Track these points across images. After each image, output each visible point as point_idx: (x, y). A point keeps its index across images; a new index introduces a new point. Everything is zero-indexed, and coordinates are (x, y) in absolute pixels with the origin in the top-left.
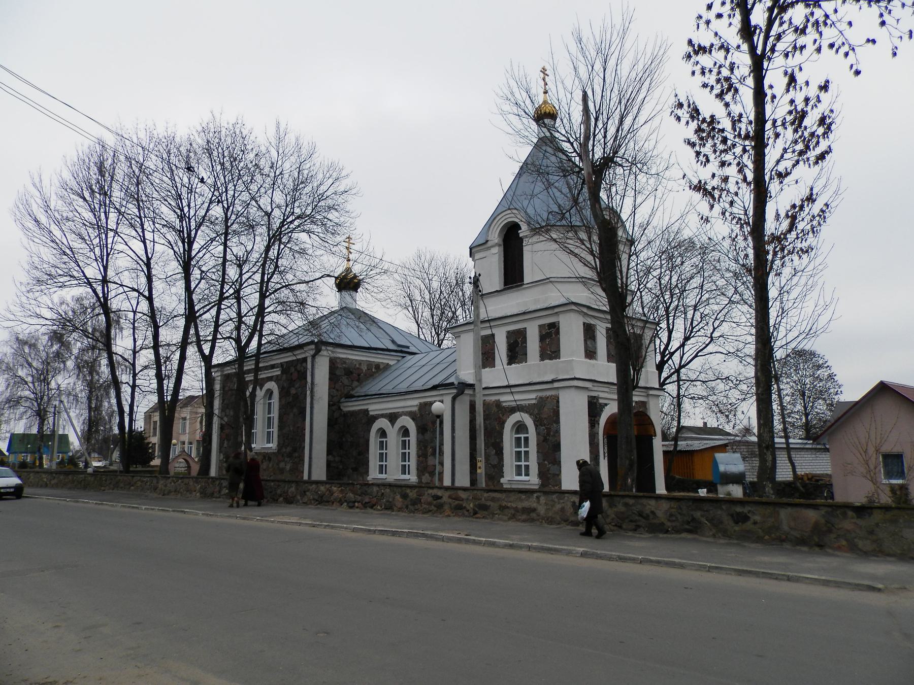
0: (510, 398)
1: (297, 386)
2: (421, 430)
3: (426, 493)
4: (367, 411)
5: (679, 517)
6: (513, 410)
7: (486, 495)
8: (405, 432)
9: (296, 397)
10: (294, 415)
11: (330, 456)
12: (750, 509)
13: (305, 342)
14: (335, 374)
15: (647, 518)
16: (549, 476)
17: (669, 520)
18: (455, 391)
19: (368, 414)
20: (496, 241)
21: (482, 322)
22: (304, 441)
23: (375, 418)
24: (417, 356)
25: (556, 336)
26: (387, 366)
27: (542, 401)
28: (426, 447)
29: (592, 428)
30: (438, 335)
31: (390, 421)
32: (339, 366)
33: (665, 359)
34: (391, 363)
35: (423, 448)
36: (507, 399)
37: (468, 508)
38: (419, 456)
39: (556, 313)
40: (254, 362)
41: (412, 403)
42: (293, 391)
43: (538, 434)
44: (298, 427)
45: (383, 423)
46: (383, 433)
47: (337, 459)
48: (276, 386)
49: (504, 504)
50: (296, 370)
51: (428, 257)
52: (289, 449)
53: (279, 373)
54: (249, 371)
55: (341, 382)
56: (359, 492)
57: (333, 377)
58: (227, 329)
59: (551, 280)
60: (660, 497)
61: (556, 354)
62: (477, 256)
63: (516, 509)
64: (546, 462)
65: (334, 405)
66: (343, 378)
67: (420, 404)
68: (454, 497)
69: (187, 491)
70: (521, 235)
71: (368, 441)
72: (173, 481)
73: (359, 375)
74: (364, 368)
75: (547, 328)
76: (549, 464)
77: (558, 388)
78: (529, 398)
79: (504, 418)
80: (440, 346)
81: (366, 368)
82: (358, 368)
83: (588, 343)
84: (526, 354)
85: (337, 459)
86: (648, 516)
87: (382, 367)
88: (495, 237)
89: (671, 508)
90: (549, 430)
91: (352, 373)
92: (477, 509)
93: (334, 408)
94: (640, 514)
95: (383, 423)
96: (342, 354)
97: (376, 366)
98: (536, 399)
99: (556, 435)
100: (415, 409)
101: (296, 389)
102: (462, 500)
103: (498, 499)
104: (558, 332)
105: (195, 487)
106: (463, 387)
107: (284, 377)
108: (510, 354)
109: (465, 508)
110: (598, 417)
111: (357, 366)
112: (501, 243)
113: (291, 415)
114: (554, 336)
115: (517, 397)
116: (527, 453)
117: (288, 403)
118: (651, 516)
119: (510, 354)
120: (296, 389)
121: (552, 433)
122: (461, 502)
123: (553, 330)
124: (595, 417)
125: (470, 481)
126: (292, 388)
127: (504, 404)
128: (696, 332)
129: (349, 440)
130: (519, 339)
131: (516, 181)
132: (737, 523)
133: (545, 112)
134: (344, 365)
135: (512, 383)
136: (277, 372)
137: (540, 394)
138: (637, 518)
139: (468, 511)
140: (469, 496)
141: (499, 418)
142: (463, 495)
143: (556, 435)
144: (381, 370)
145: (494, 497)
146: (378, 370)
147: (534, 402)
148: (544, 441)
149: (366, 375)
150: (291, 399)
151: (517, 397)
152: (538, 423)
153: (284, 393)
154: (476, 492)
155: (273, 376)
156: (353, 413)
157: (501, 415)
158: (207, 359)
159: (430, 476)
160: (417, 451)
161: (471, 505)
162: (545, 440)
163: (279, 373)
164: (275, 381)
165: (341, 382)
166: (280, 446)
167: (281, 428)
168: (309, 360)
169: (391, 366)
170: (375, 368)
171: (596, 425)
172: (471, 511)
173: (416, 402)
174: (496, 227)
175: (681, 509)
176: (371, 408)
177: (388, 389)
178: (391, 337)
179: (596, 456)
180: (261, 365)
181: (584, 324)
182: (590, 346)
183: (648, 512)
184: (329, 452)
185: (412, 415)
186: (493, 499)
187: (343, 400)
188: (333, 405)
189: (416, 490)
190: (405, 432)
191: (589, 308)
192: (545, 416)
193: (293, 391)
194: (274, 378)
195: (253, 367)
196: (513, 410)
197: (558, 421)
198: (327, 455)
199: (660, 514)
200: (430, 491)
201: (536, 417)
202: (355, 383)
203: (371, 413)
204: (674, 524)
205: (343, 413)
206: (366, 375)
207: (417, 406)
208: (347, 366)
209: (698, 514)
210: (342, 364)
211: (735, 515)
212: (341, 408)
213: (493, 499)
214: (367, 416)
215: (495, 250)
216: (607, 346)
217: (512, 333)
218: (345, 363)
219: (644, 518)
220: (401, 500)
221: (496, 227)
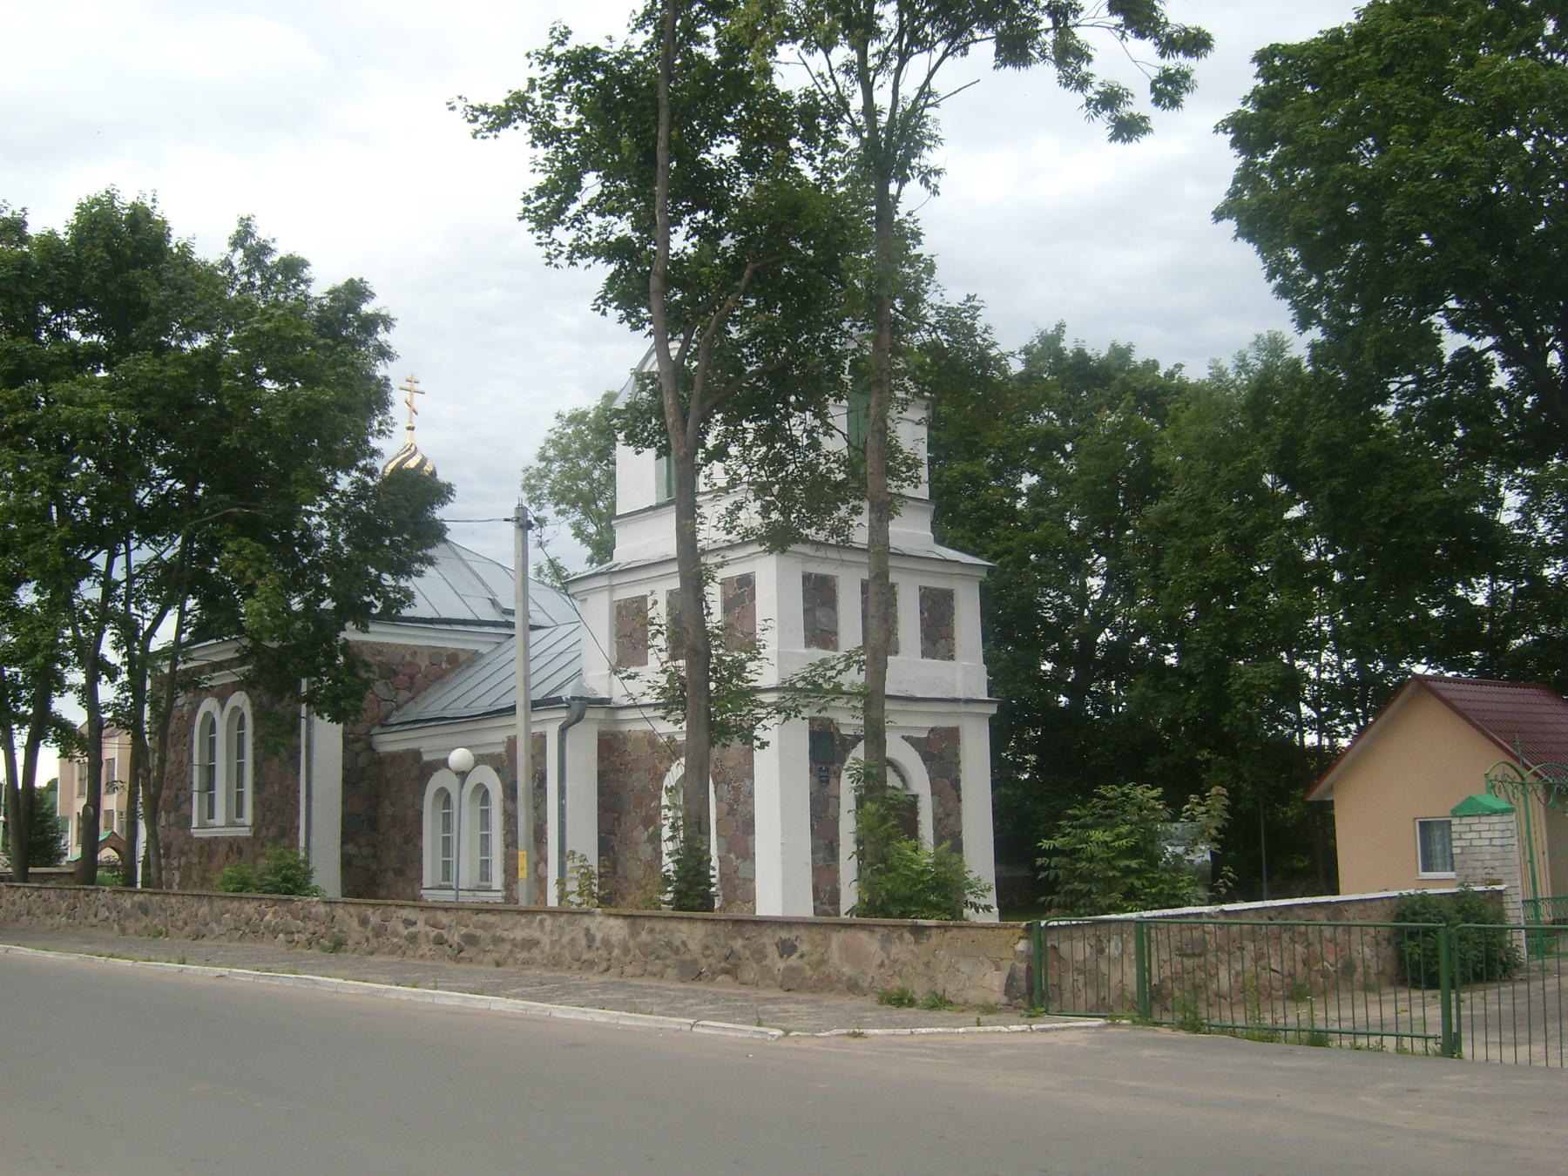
4: (417, 754)
5: (715, 949)
7: (475, 918)
15: (677, 951)
18: (563, 714)
26: (475, 657)
34: (483, 649)
37: (450, 941)
39: (750, 555)
46: (444, 797)
48: (248, 703)
49: (499, 933)
52: (273, 831)
58: (1349, 61)
63: (514, 942)
64: (732, 856)
69: (48, 913)
71: (420, 814)
72: (25, 894)
73: (412, 677)
74: (423, 662)
81: (427, 663)
82: (410, 664)
85: (367, 851)
86: (677, 947)
87: (462, 657)
90: (737, 790)
91: (395, 673)
93: (358, 746)
94: (669, 944)
97: (448, 656)
105: (59, 905)
106: (583, 705)
111: (408, 658)
129: (389, 813)
144: (459, 665)
145: (485, 923)
146: (456, 662)
148: (728, 814)
154: (461, 913)
160: (505, 835)
167: (258, 787)
169: (482, 656)
171: (833, 781)
172: (455, 946)
175: (717, 936)
177: (458, 709)
178: (491, 592)
179: (831, 842)
181: (807, 578)
184: (347, 837)
187: (376, 730)
192: (731, 764)
198: (344, 843)
202: (404, 695)
203: (426, 758)
209: (738, 944)
210: (374, 655)
213: (485, 926)
218: (380, 653)
220: (359, 929)
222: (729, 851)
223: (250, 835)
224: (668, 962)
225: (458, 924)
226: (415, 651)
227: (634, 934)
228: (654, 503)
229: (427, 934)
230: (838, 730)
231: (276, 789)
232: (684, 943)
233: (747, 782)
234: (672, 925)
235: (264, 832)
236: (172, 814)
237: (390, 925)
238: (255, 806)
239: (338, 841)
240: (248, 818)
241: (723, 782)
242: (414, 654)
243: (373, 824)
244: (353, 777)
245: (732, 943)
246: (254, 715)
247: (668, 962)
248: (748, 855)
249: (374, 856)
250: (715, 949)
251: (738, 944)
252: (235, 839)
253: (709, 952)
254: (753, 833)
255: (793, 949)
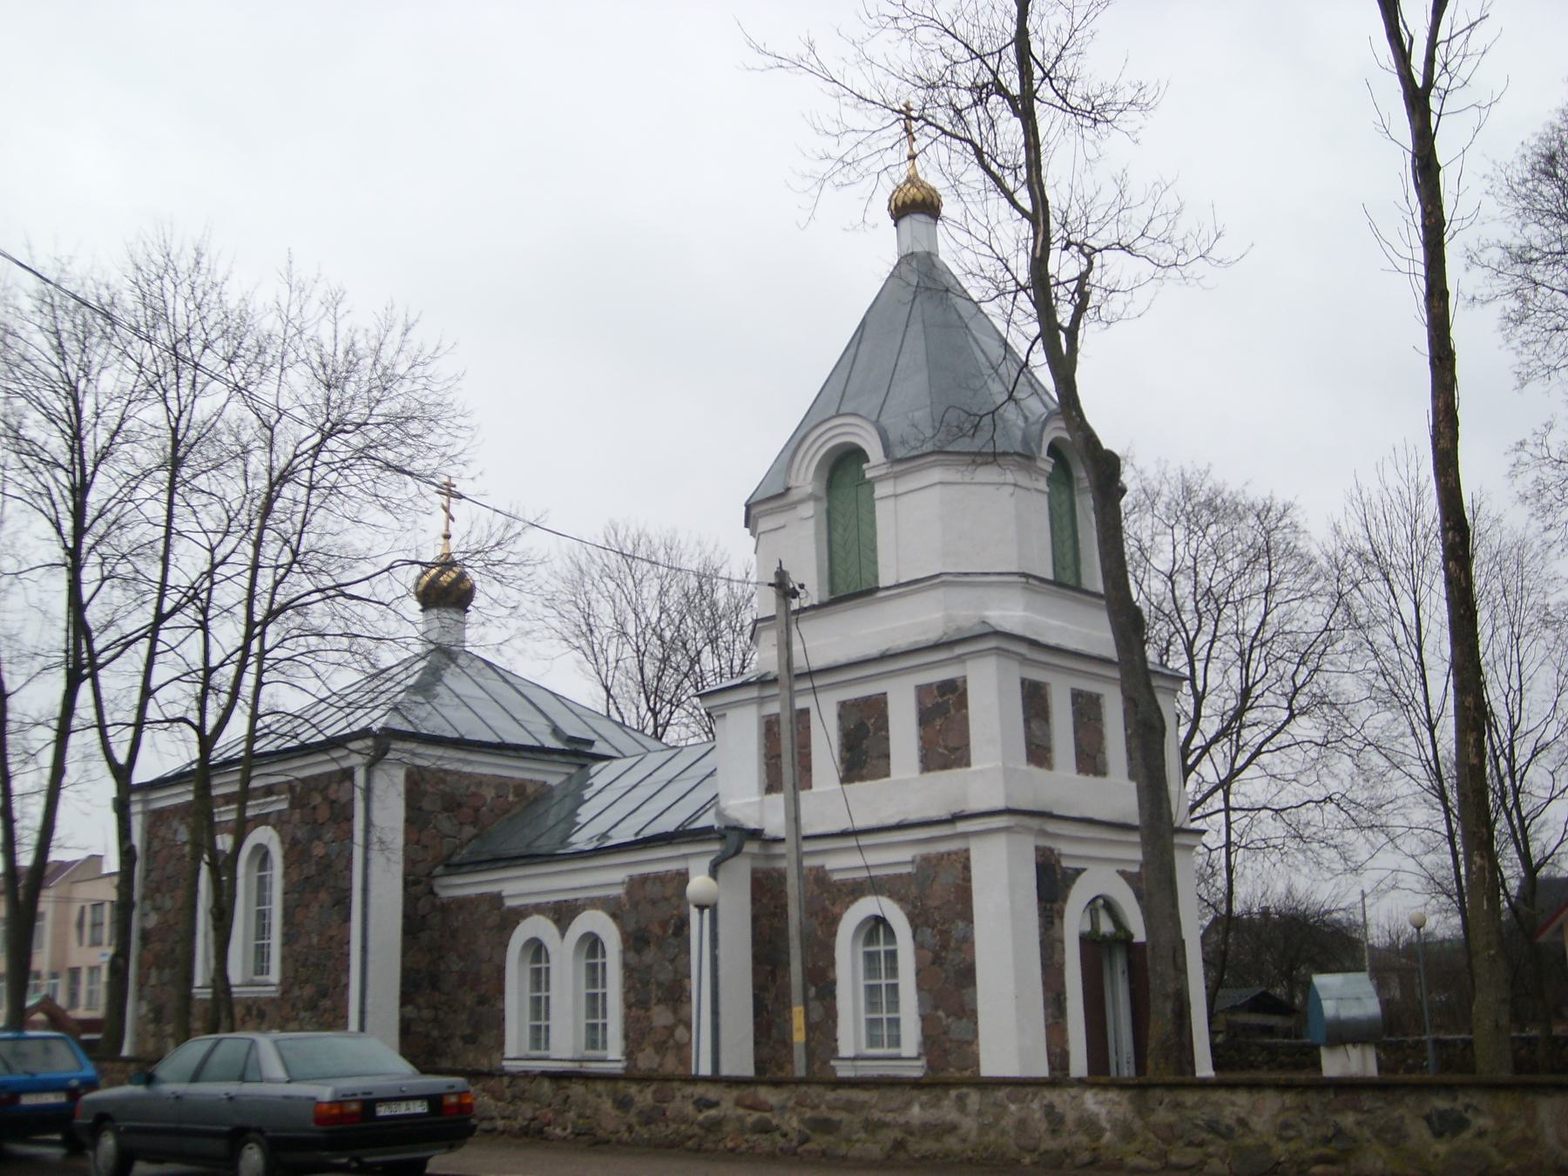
0: (855, 860)
1: (328, 836)
2: (635, 941)
3: (679, 1095)
4: (497, 898)
5: (1304, 1128)
6: (857, 890)
7: (830, 1095)
8: (592, 944)
9: (326, 865)
10: (321, 907)
11: (409, 1008)
12: (1467, 1100)
13: (347, 731)
14: (420, 809)
15: (1228, 1134)
16: (948, 1045)
17: (1281, 1138)
18: (716, 847)
19: (502, 904)
20: (809, 489)
21: (800, 676)
22: (347, 970)
23: (520, 914)
24: (615, 762)
25: (958, 710)
27: (929, 866)
28: (646, 984)
29: (1046, 929)
30: (655, 714)
31: (557, 922)
32: (429, 789)
33: (1190, 762)
34: (554, 781)
35: (638, 986)
36: (843, 864)
37: (785, 1128)
38: (628, 1006)
39: (959, 657)
40: (237, 777)
41: (611, 877)
42: (318, 850)
43: (919, 946)
44: (331, 938)
45: (538, 927)
46: (536, 949)
47: (427, 1014)
49: (876, 1115)
50: (325, 798)
51: (633, 531)
52: (308, 991)
53: (284, 806)
54: (228, 799)
55: (435, 827)
56: (508, 1093)
57: (415, 818)
59: (944, 578)
60: (1205, 1084)
61: (958, 753)
62: (764, 524)
64: (941, 1013)
65: (416, 884)
66: (440, 816)
67: (631, 878)
68: (748, 1102)
70: (868, 475)
73: (477, 810)
74: (489, 794)
75: (936, 692)
76: (948, 1016)
77: (965, 835)
78: (897, 857)
79: (836, 910)
80: (658, 737)
82: (474, 795)
83: (1032, 725)
84: (888, 756)
85: (427, 1014)
86: (1230, 1129)
88: (806, 479)
89: (1284, 1109)
91: (460, 805)
92: (808, 1132)
95: (538, 927)
96: (430, 758)
98: (913, 862)
99: (964, 946)
100: (619, 891)
101: (326, 843)
102: (771, 1109)
103: (863, 1105)
104: (962, 702)
107: (297, 815)
108: (848, 755)
109: (777, 1128)
110: (1060, 903)
112: (822, 493)
113: (315, 909)
114: (953, 711)
115: (873, 858)
116: (893, 989)
117: (307, 878)
118: (1239, 1130)
119: (848, 755)
120: (326, 843)
121: (952, 944)
122: (768, 1115)
123: (951, 698)
124: (1053, 901)
125: (756, 1063)
126: (316, 843)
127: (836, 877)
128: (1257, 698)
129: (456, 968)
130: (869, 718)
131: (852, 351)
132: (1438, 1134)
133: (904, 203)
134: (441, 786)
135: (860, 824)
136: (280, 804)
137: (637, 871)
138: (1204, 1135)
139: (785, 1135)
140: (789, 1098)
141: (824, 909)
142: (728, 1097)
143: (964, 946)
147: (908, 869)
148: (934, 963)
149: (492, 811)
150: (314, 868)
151: (873, 858)
152: (917, 921)
153: (295, 853)
155: (268, 814)
156: (463, 903)
157: (827, 902)
158: (122, 773)
159: (657, 1053)
161: (795, 1123)
162: (937, 960)
163: (284, 806)
164: (274, 827)
165: (435, 827)
166: (287, 983)
167: (288, 939)
168: (360, 777)
170: (516, 795)
171: (1057, 921)
173: (620, 875)
174: (806, 461)
175: (1307, 1109)
176: (508, 889)
180: (254, 784)
181: (1023, 681)
182: (1038, 733)
183: (1231, 1121)
184: (406, 998)
185: (614, 909)
186: (849, 1107)
187: (439, 870)
188: (417, 883)
189: (653, 1087)
190: (592, 944)
191: (1034, 644)
192: (937, 903)
193: (318, 850)
194: (272, 819)
195: (236, 788)
196: (857, 890)
197: (967, 916)
198: (403, 1003)
199: (1260, 1123)
200: (689, 1090)
201: (915, 907)
203: (509, 903)
204: (1293, 1146)
205: (438, 902)
206: (492, 811)
207: (623, 883)
208: (448, 789)
209: (1348, 1120)
211: (1434, 1118)
212: (436, 889)
214: (499, 909)
215: (808, 510)
216: (1076, 732)
217: (853, 705)
219: (1223, 1136)
220: (615, 1112)
221: (806, 461)
222: (936, 1008)
223: (277, 995)
224: (1211, 1149)
225: (800, 1104)
226: (480, 780)
227: (1142, 1111)
228: (815, 602)
229: (740, 1119)
230: (1059, 862)
231: (315, 940)
232: (1242, 1122)
233: (961, 924)
234: (1220, 1096)
235: (296, 992)
236: (167, 971)
237: (671, 1108)
238: (284, 959)
239: (396, 1002)
240: (275, 976)
241: (926, 923)
242: (480, 784)
243: (434, 982)
244: (413, 926)
245: (1338, 1118)
246: (286, 857)
247: (1211, 1149)
248: (968, 1013)
249: (436, 1020)
250: (1304, 1128)
251: (1348, 1120)
252: (256, 1000)
253: (1291, 1133)
254: (974, 984)
255: (1460, 1124)
